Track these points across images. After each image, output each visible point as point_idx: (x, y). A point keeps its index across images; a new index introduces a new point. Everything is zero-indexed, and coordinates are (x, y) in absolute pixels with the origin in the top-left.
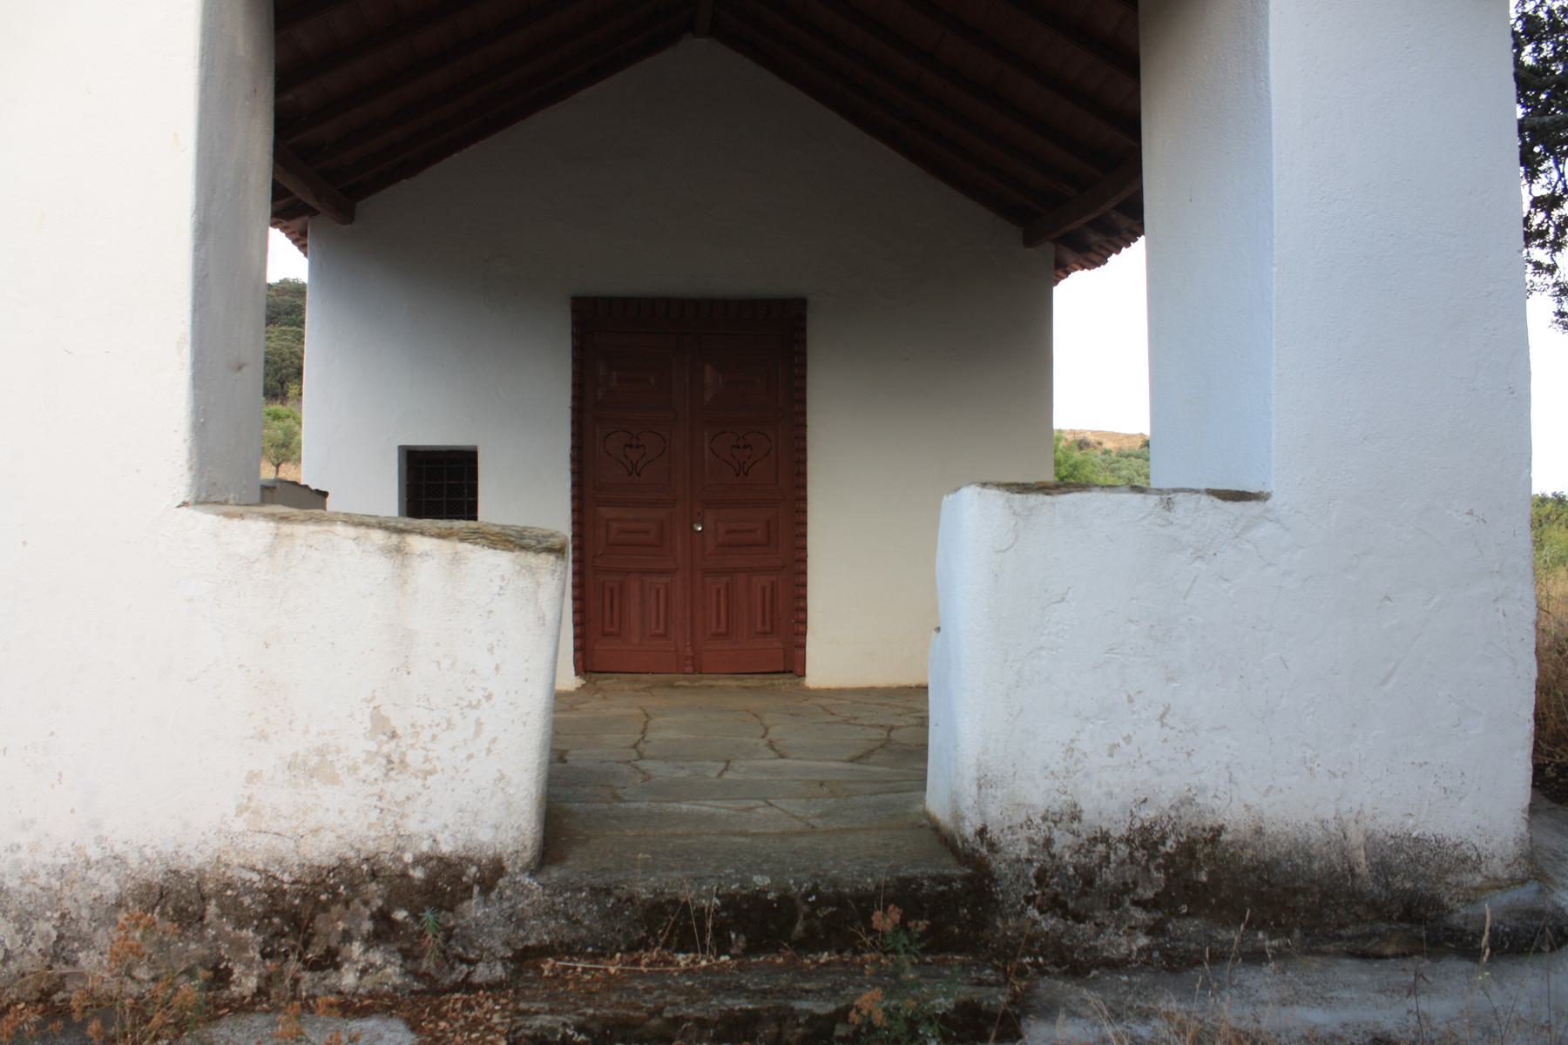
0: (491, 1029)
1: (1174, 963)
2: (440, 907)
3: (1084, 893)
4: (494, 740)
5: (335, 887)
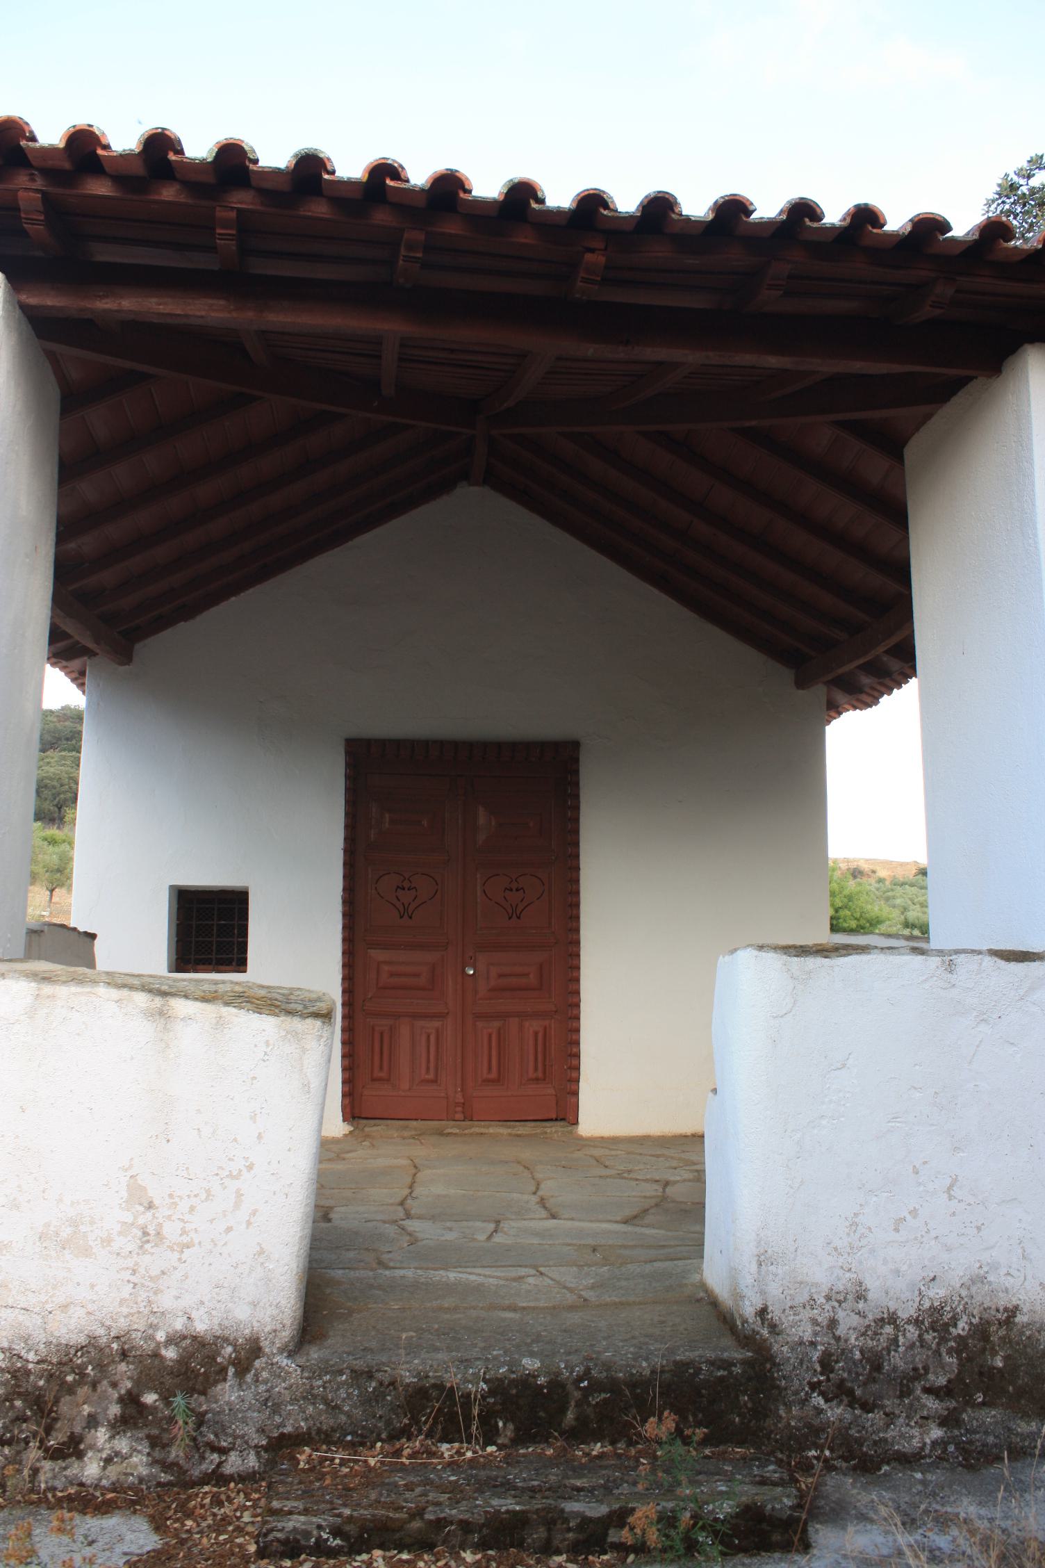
0: (240, 1530)
1: (972, 1459)
2: (191, 1391)
3: (871, 1379)
4: (254, 1213)
5: (82, 1367)
